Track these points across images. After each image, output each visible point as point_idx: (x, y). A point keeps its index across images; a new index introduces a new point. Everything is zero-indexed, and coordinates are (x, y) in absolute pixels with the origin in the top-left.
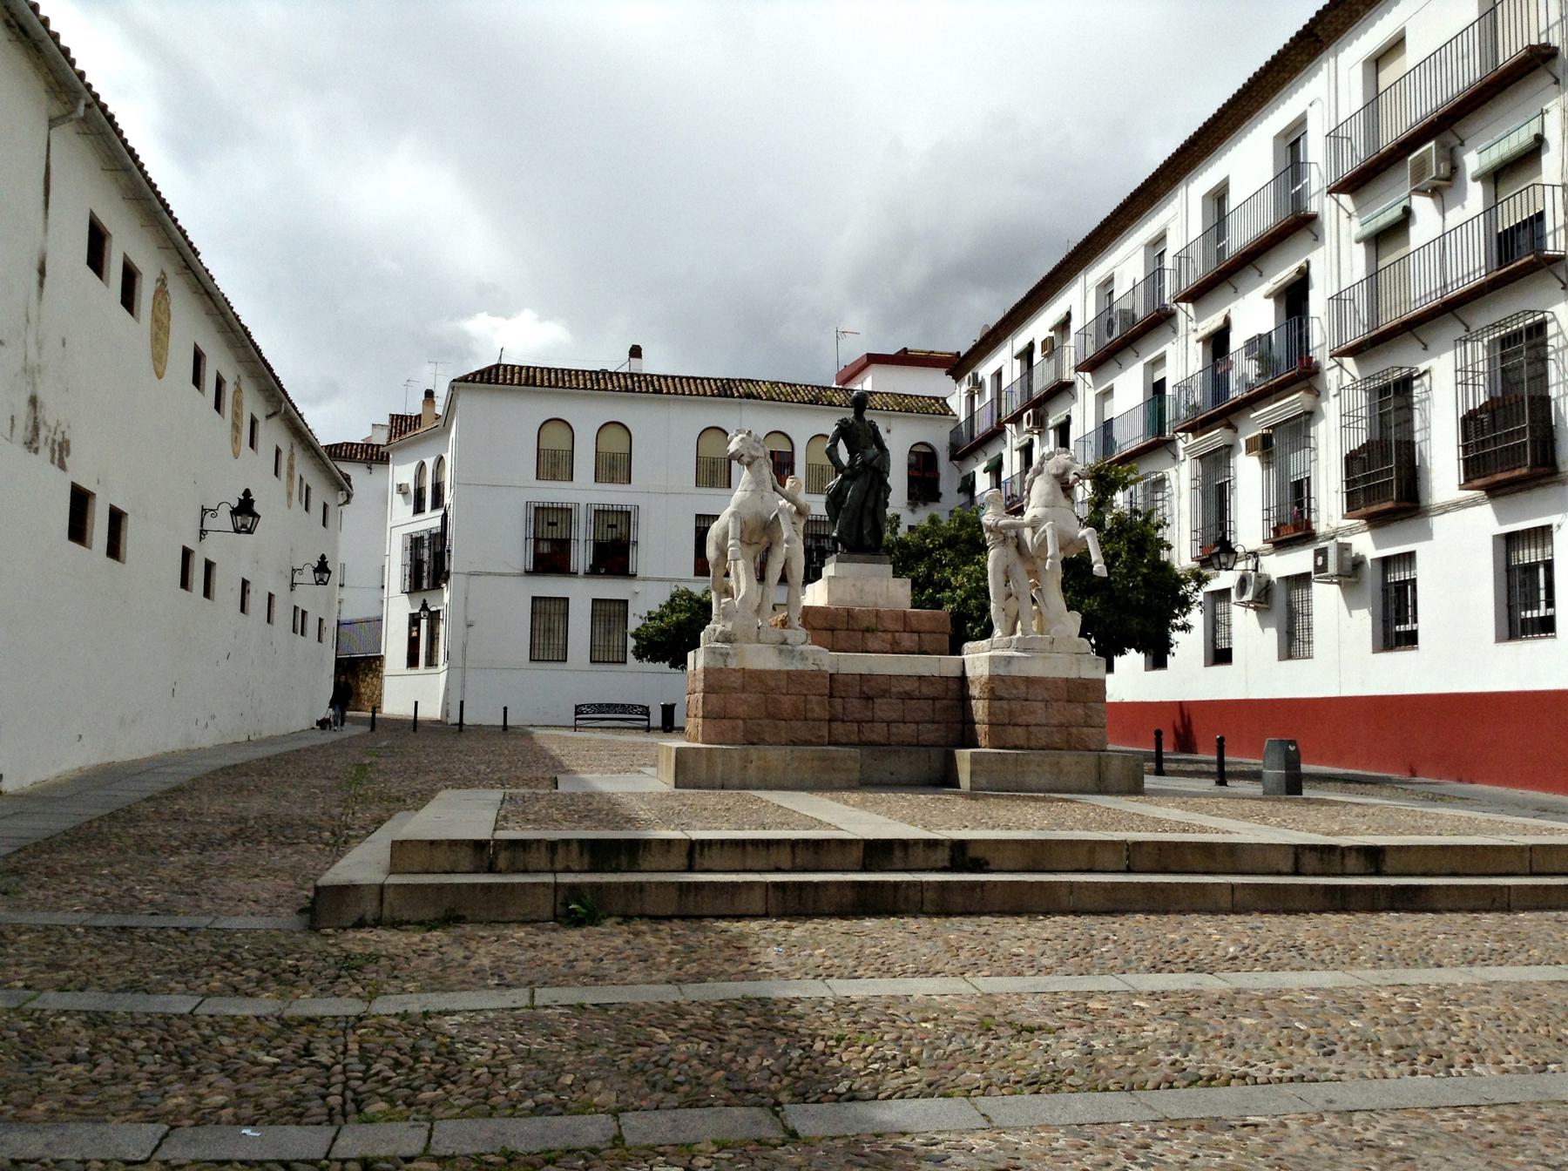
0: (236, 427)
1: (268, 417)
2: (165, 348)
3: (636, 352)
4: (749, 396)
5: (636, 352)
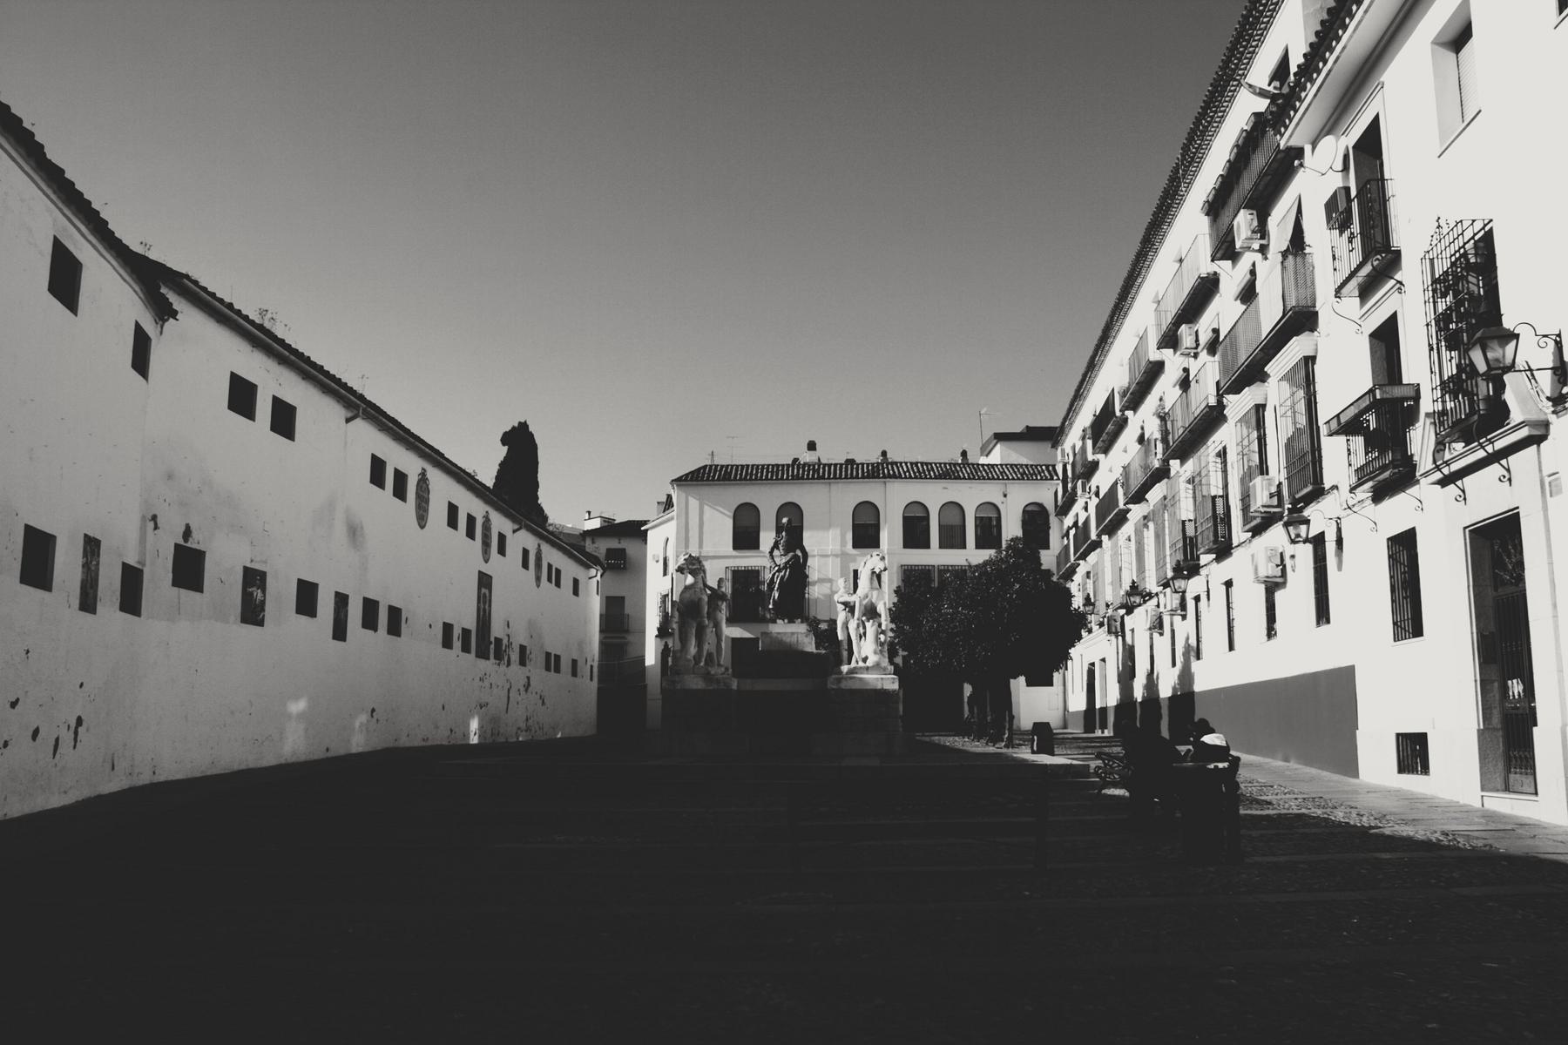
0: (486, 544)
1: (348, 420)
2: (426, 510)
3: (812, 446)
4: (894, 476)
5: (812, 446)
